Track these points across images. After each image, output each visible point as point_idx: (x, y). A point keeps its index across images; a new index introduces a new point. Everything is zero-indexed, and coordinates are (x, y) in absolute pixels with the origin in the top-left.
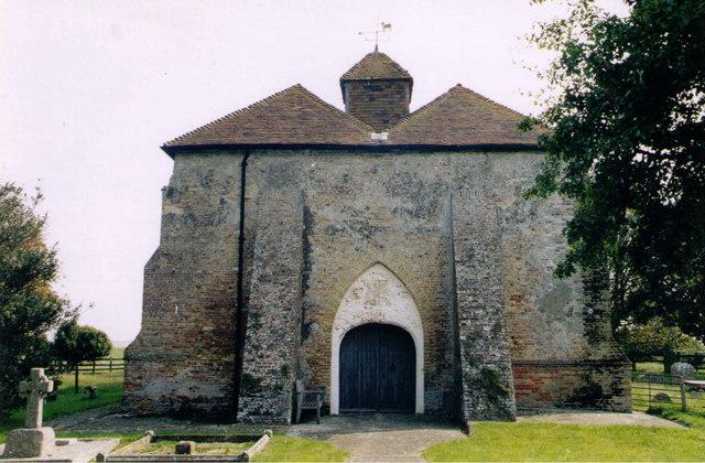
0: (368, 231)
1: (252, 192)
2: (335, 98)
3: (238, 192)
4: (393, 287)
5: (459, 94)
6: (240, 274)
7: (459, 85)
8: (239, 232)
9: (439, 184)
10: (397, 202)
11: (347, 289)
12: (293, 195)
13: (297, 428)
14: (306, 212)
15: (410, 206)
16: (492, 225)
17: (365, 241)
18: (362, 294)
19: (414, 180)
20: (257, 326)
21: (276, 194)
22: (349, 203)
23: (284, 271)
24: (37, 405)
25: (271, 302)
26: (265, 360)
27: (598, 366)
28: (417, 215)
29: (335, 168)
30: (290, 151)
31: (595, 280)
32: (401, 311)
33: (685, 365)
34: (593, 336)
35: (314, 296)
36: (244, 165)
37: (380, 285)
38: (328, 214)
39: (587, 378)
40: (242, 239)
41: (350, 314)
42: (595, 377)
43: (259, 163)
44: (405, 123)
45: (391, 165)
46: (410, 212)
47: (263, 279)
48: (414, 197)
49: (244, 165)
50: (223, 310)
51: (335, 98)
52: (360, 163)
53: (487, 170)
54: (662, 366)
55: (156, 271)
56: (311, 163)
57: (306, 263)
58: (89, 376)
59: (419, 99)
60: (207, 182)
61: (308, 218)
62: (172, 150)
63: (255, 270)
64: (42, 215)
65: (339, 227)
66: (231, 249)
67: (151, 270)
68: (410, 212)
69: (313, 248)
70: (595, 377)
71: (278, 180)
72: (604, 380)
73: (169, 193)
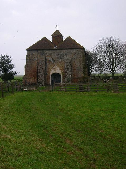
0: (54, 61)
1: (38, 56)
2: (51, 39)
4: (58, 68)
5: (69, 39)
6: (37, 67)
9: (64, 54)
10: (58, 56)
12: (44, 56)
14: (46, 58)
15: (60, 57)
16: (70, 60)
18: (54, 69)
20: (57, 103)
21: (41, 56)
23: (43, 67)
25: (41, 71)
26: (41, 78)
27: (85, 78)
28: (60, 58)
29: (49, 52)
32: (59, 71)
33: (111, 78)
34: (84, 74)
35: (47, 70)
36: (37, 52)
37: (56, 68)
38: (49, 58)
41: (52, 72)
42: (85, 80)
43: (39, 52)
44: (62, 42)
45: (49, 61)
47: (40, 68)
48: (60, 56)
50: (35, 72)
51: (51, 39)
52: (53, 51)
53: (70, 51)
55: (26, 67)
56: (46, 52)
60: (32, 54)
61: (46, 59)
62: (26, 50)
63: (39, 67)
64: (10, 60)
66: (36, 64)
67: (25, 67)
70: (85, 80)
71: (42, 54)
72: (86, 80)
73: (27, 56)
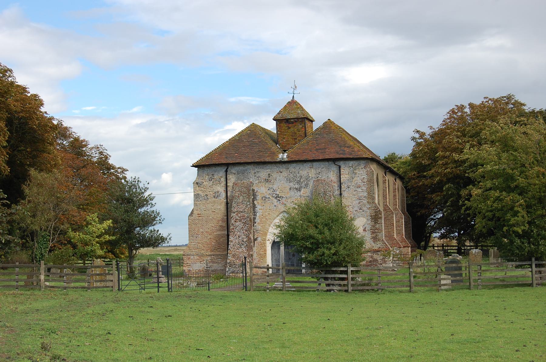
3: (225, 183)
7: (329, 120)
8: (226, 200)
11: (271, 223)
13: (344, 293)
15: (297, 186)
17: (278, 202)
19: (298, 175)
22: (271, 186)
24: (9, 202)
30: (246, 165)
31: (376, 215)
36: (226, 171)
39: (372, 257)
40: (227, 203)
42: (375, 256)
43: (234, 170)
46: (297, 189)
49: (226, 171)
54: (442, 247)
57: (254, 212)
58: (312, 241)
59: (316, 126)
65: (268, 197)
68: (297, 189)
69: (257, 206)
70: (375, 256)
